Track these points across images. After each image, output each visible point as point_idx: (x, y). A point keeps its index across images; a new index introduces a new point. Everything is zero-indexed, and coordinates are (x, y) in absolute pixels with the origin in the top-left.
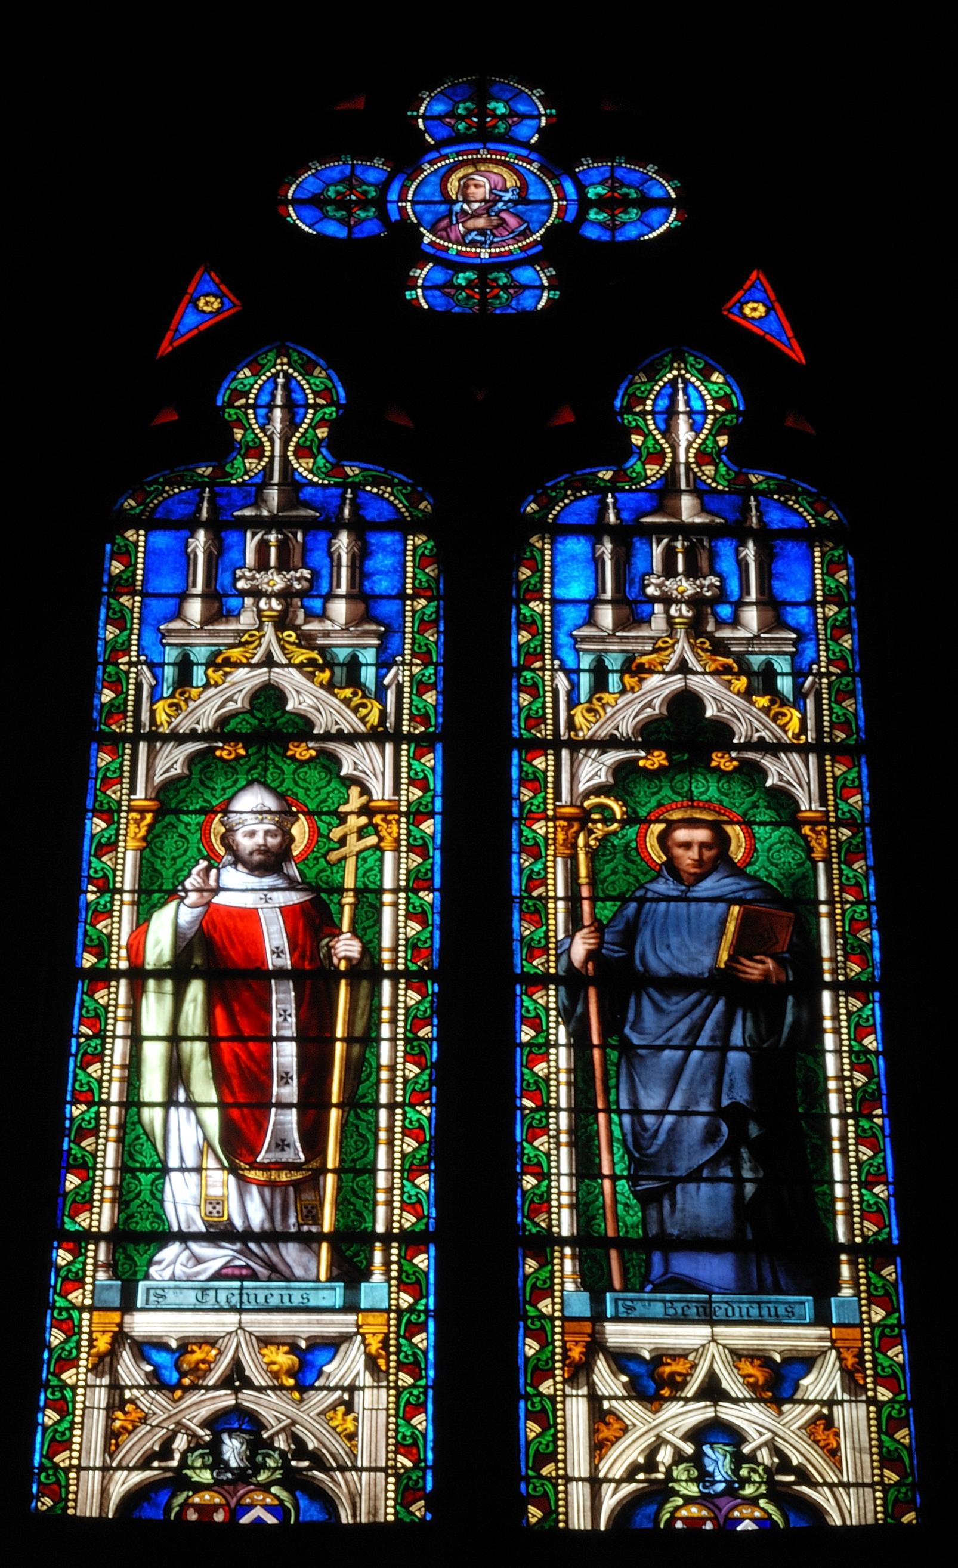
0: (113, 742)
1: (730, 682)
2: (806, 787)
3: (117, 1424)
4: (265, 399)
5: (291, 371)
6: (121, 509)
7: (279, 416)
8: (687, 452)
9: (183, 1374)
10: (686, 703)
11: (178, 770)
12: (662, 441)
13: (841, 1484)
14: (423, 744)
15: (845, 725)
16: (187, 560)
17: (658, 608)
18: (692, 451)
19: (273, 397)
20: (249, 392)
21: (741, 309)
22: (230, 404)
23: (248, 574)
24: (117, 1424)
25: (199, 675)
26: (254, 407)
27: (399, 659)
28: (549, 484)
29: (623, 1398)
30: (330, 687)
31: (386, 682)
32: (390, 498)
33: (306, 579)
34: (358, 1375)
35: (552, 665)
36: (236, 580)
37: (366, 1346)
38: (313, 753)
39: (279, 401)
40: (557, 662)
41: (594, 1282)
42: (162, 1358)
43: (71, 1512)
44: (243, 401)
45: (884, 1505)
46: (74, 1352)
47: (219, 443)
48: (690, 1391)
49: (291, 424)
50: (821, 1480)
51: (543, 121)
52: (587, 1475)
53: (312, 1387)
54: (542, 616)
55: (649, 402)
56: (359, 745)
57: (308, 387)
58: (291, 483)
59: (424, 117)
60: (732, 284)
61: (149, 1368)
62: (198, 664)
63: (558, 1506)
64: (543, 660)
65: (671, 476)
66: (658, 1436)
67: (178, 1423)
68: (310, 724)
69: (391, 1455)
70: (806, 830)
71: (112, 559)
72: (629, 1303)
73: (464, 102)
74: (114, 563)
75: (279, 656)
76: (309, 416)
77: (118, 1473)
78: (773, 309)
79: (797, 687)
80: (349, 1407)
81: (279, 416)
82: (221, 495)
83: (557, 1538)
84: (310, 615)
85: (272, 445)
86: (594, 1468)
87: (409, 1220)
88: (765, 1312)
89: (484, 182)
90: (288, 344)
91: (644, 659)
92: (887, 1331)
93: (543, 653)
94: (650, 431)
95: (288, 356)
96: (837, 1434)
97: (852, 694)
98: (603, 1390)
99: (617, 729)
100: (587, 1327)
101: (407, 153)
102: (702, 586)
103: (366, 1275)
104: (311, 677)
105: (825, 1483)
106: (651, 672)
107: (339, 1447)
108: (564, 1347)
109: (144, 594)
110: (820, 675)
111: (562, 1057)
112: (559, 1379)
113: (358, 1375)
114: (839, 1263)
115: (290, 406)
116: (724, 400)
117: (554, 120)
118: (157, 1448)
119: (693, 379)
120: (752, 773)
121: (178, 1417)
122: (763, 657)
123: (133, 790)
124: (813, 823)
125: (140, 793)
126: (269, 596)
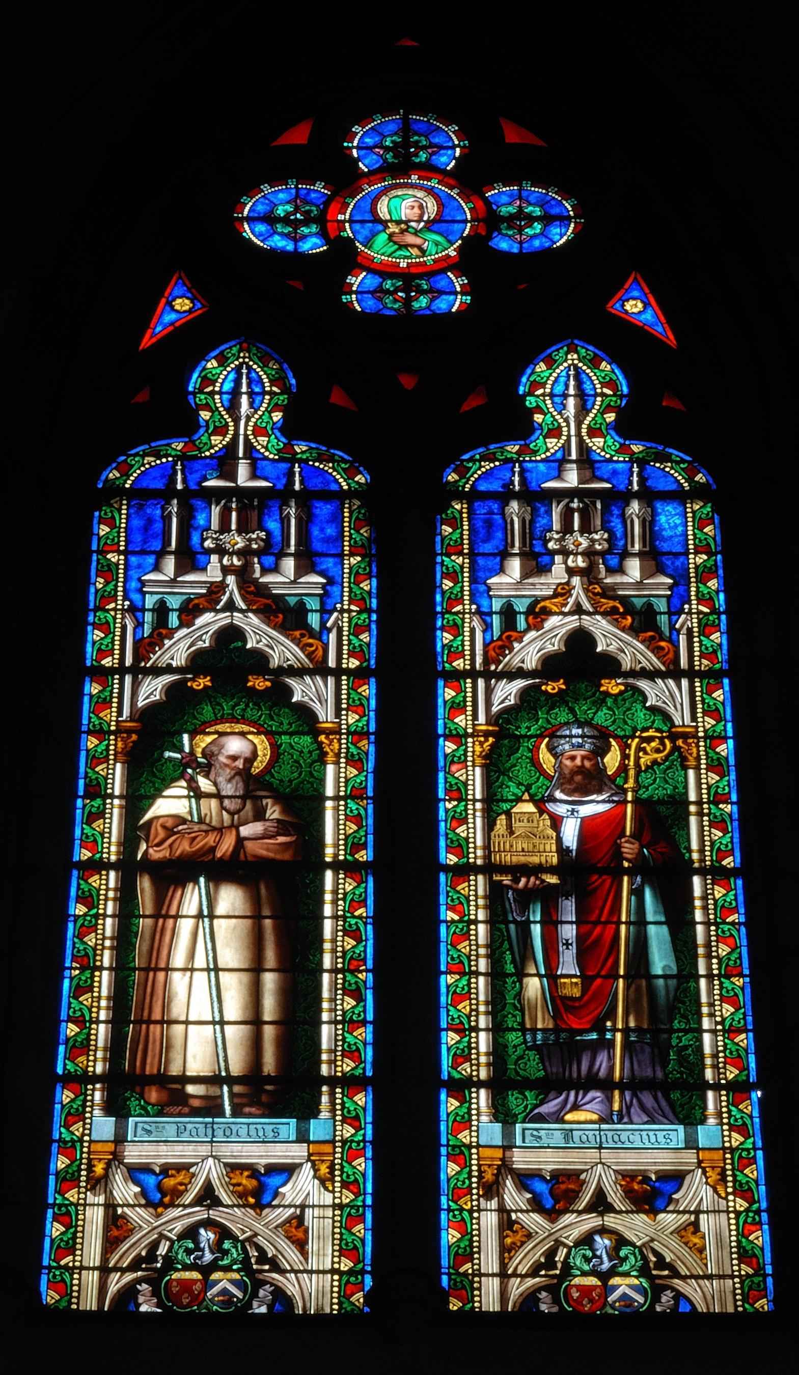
0: (102, 674)
1: (616, 620)
2: (679, 707)
3: (508, 1241)
4: (559, 389)
5: (580, 365)
6: (448, 482)
7: (241, 404)
8: (246, 425)
9: (164, 1195)
10: (580, 640)
11: (157, 697)
12: (226, 416)
13: (306, 1271)
14: (712, 677)
15: (711, 655)
16: (506, 527)
17: (214, 558)
18: (251, 424)
19: (567, 386)
20: (545, 383)
21: (623, 306)
22: (531, 393)
23: (556, 536)
24: (508, 1241)
25: (174, 620)
26: (552, 395)
27: (338, 606)
28: (466, 457)
29: (527, 1211)
30: (633, 630)
31: (329, 625)
32: (673, 473)
33: (262, 540)
34: (308, 1194)
35: (123, 605)
36: (203, 540)
37: (707, 1178)
38: (623, 688)
39: (572, 391)
40: (474, 607)
41: (502, 1114)
42: (151, 1181)
43: (74, 1307)
44: (210, 388)
45: (339, 1286)
46: (467, 1182)
47: (520, 425)
48: (189, 1198)
49: (583, 410)
50: (289, 1268)
51: (458, 150)
52: (97, 1264)
53: (269, 1205)
54: (117, 564)
55: (218, 384)
56: (659, 681)
57: (594, 379)
58: (586, 461)
59: (359, 148)
60: (614, 287)
61: (529, 1196)
62: (173, 610)
63: (72, 1291)
64: (116, 601)
65: (232, 445)
66: (556, 1241)
67: (556, 1241)
68: (618, 663)
69: (336, 1259)
70: (322, 738)
71: (99, 523)
72: (535, 1133)
73: (391, 135)
74: (102, 526)
75: (587, 606)
76: (598, 403)
77: (513, 1280)
78: (650, 304)
79: (323, 623)
80: (696, 1225)
81: (241, 404)
82: (528, 471)
83: (68, 1318)
84: (610, 571)
85: (568, 426)
86: (503, 1265)
87: (348, 1066)
88: (253, 1132)
89: (403, 204)
90: (576, 342)
91: (547, 603)
92: (744, 1154)
93: (116, 596)
94: (217, 408)
95: (577, 352)
96: (703, 1237)
97: (368, 628)
98: (509, 1203)
99: (523, 662)
100: (499, 1154)
101: (345, 179)
102: (593, 541)
103: (315, 1114)
104: (616, 623)
105: (293, 1271)
106: (550, 613)
107: (690, 1258)
108: (479, 1171)
109: (126, 553)
110: (342, 611)
111: (109, 926)
112: (475, 1197)
113: (308, 1194)
114: (320, 1094)
115: (581, 395)
116: (611, 384)
117: (467, 151)
118: (144, 1253)
119: (255, 367)
120: (281, 693)
121: (159, 1229)
122: (645, 600)
123: (475, 716)
124: (328, 732)
125: (482, 718)
126: (231, 554)
